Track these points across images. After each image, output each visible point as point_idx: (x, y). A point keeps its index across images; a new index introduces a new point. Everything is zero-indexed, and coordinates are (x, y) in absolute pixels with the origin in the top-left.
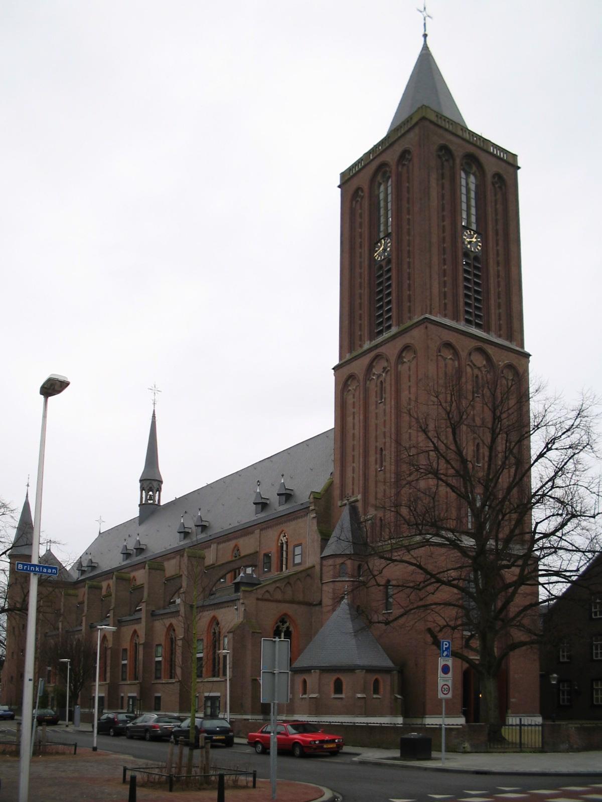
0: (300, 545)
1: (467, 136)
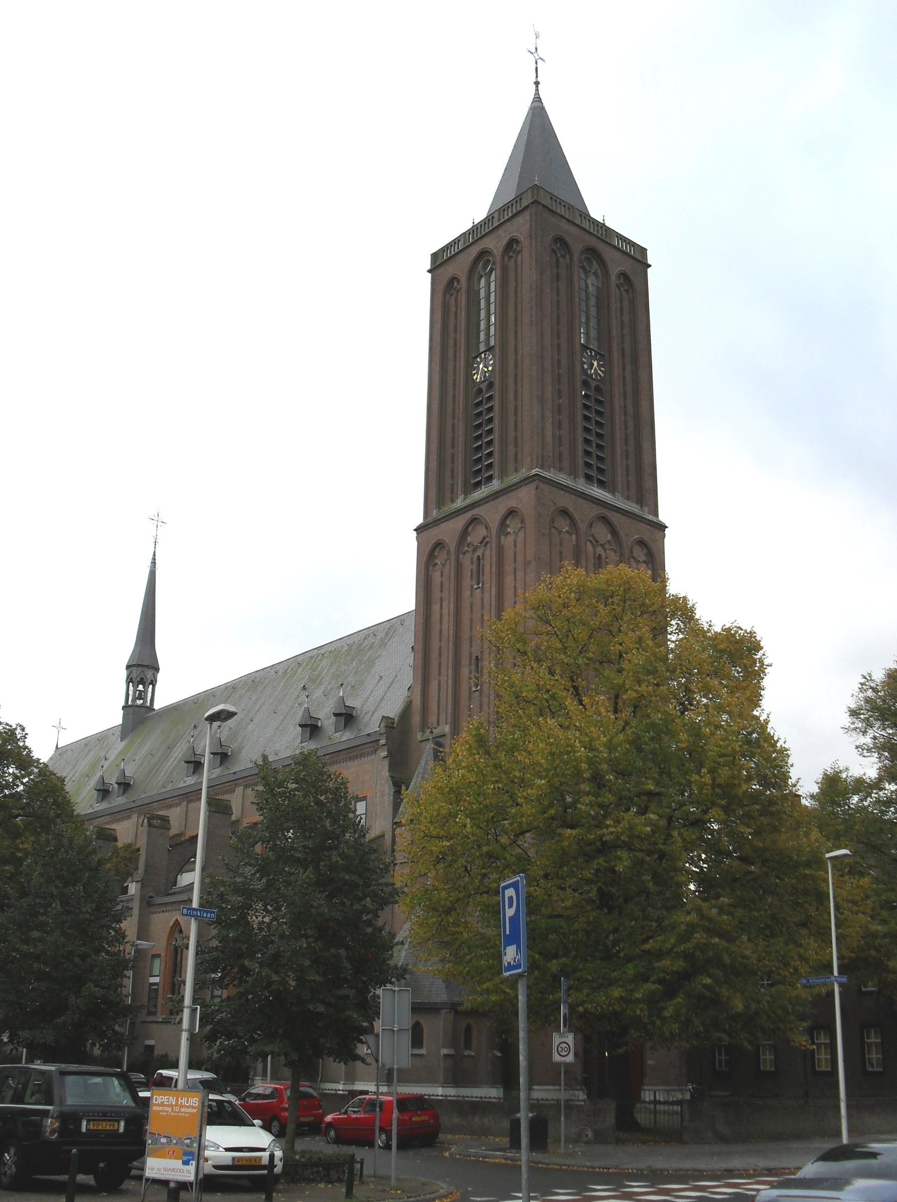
0: (364, 798)
1: (586, 225)
